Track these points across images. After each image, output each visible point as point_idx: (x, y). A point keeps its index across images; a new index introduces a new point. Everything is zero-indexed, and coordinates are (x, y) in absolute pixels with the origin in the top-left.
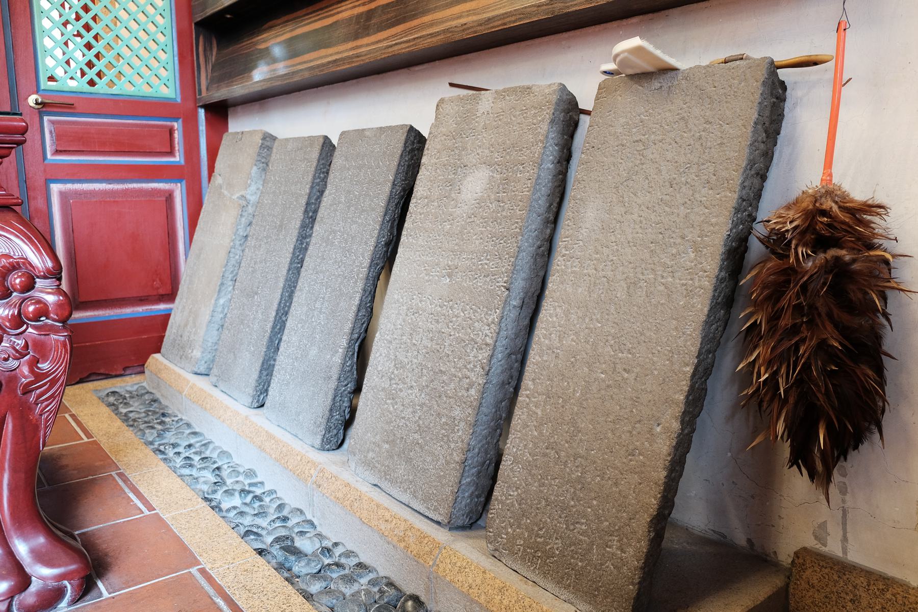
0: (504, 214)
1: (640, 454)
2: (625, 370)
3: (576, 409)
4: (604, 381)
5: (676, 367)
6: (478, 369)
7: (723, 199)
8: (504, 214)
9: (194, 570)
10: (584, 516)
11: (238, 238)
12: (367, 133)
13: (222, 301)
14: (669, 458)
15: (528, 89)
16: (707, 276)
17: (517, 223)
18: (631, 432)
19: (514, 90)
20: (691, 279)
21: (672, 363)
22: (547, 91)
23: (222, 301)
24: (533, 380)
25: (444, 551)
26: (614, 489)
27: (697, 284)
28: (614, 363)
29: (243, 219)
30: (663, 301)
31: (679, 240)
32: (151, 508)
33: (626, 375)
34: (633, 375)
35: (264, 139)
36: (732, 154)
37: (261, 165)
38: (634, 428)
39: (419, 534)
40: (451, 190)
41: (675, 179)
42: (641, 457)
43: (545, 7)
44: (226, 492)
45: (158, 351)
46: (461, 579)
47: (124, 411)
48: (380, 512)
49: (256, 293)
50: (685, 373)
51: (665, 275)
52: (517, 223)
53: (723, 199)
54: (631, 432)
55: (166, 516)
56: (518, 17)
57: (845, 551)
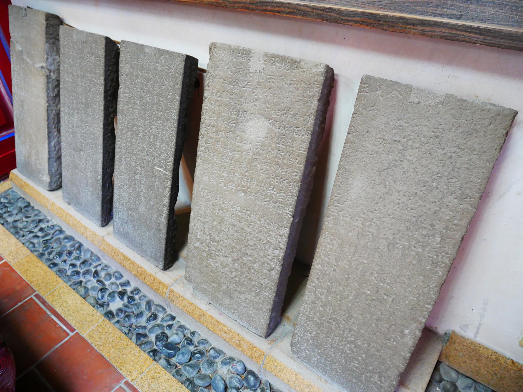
0: (285, 161)
1: (394, 341)
2: (385, 294)
3: (350, 305)
4: (369, 295)
5: (421, 303)
6: (276, 260)
7: (466, 210)
8: (285, 161)
9: (122, 384)
10: (357, 360)
11: (51, 99)
12: (147, 50)
13: (53, 144)
14: (413, 349)
15: (294, 63)
16: (447, 257)
17: (297, 172)
18: (388, 329)
19: (283, 59)
20: (437, 256)
21: (419, 301)
22: (314, 70)
23: (53, 144)
24: (318, 279)
25: (268, 358)
26: (376, 353)
27: (440, 260)
28: (377, 288)
29: (50, 85)
30: (414, 262)
31: (429, 227)
32: (73, 330)
33: (385, 297)
34: (391, 299)
35: (47, 20)
36: (476, 180)
37: (51, 41)
38: (390, 327)
39: (249, 344)
40: (235, 127)
41: (428, 182)
42: (395, 343)
43: (319, 12)
44: (110, 294)
45: (14, 166)
46: (282, 375)
47: (10, 220)
48: (220, 326)
49: (81, 150)
50: (427, 308)
51: (417, 246)
52: (297, 172)
53: (466, 210)
54: (388, 329)
55: (84, 335)
56: (291, 10)
57: (475, 336)
